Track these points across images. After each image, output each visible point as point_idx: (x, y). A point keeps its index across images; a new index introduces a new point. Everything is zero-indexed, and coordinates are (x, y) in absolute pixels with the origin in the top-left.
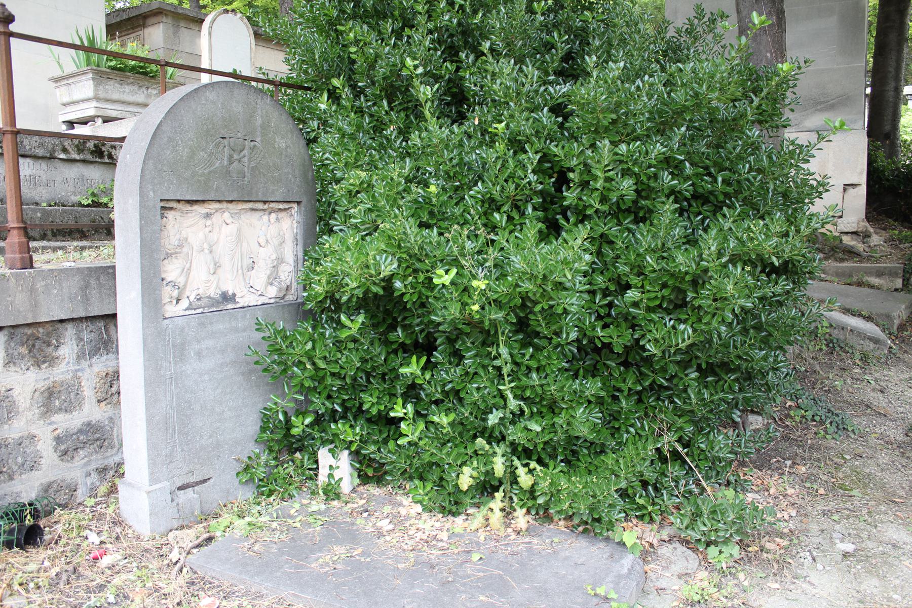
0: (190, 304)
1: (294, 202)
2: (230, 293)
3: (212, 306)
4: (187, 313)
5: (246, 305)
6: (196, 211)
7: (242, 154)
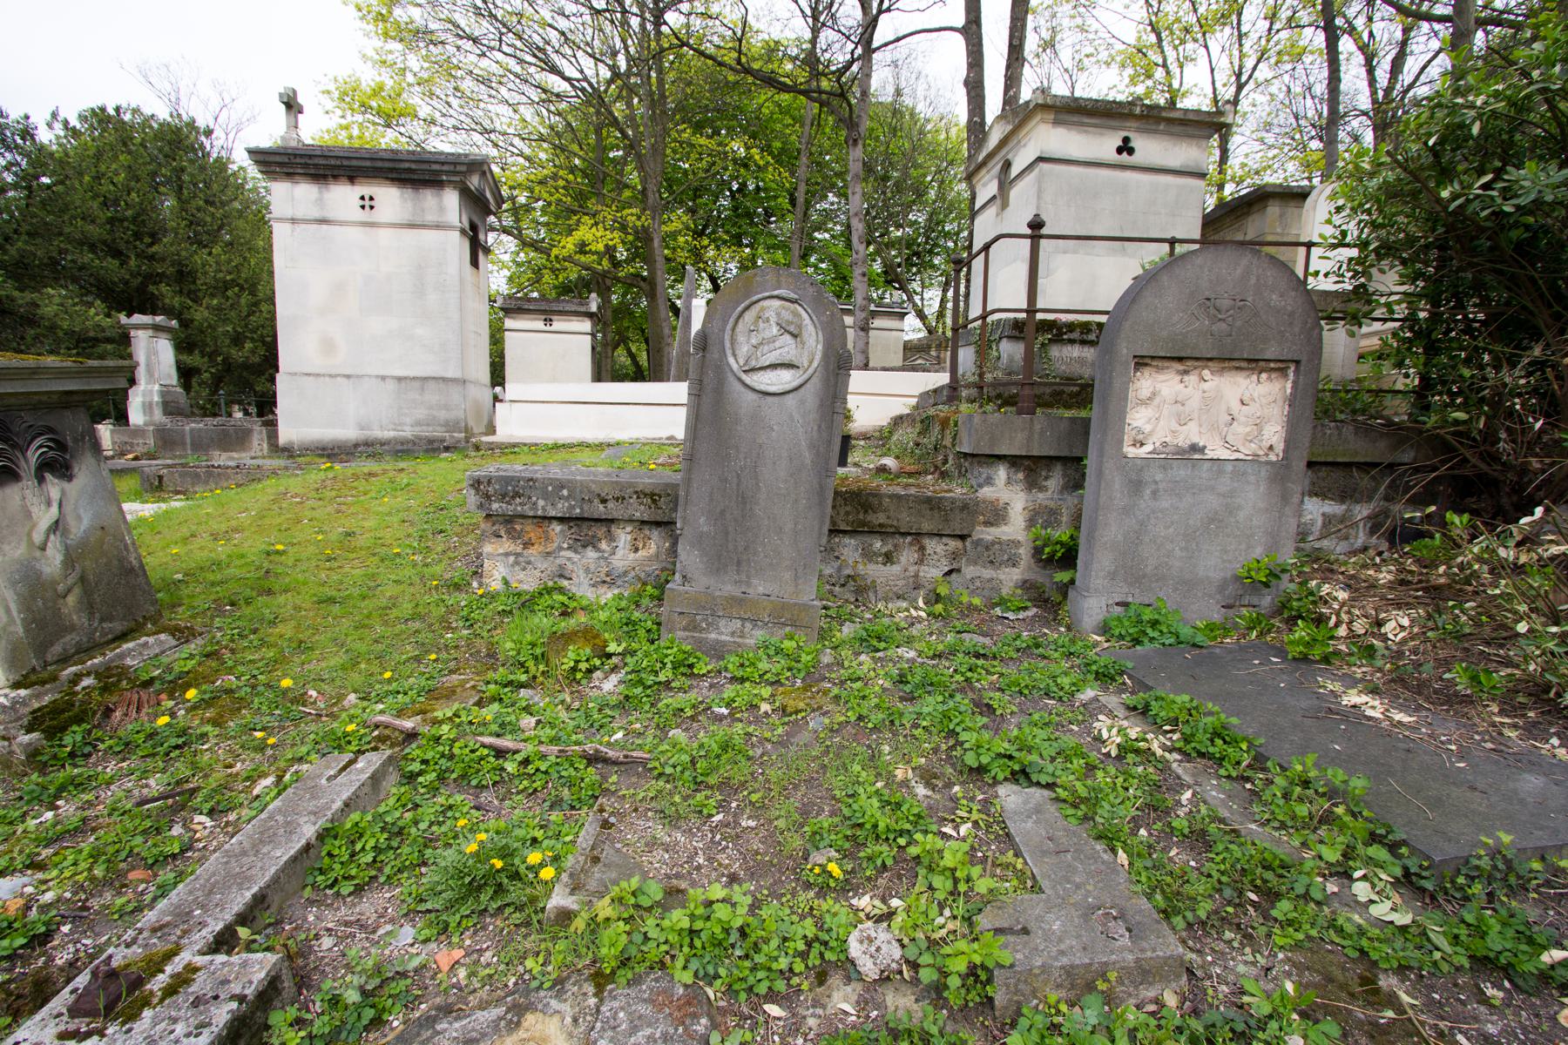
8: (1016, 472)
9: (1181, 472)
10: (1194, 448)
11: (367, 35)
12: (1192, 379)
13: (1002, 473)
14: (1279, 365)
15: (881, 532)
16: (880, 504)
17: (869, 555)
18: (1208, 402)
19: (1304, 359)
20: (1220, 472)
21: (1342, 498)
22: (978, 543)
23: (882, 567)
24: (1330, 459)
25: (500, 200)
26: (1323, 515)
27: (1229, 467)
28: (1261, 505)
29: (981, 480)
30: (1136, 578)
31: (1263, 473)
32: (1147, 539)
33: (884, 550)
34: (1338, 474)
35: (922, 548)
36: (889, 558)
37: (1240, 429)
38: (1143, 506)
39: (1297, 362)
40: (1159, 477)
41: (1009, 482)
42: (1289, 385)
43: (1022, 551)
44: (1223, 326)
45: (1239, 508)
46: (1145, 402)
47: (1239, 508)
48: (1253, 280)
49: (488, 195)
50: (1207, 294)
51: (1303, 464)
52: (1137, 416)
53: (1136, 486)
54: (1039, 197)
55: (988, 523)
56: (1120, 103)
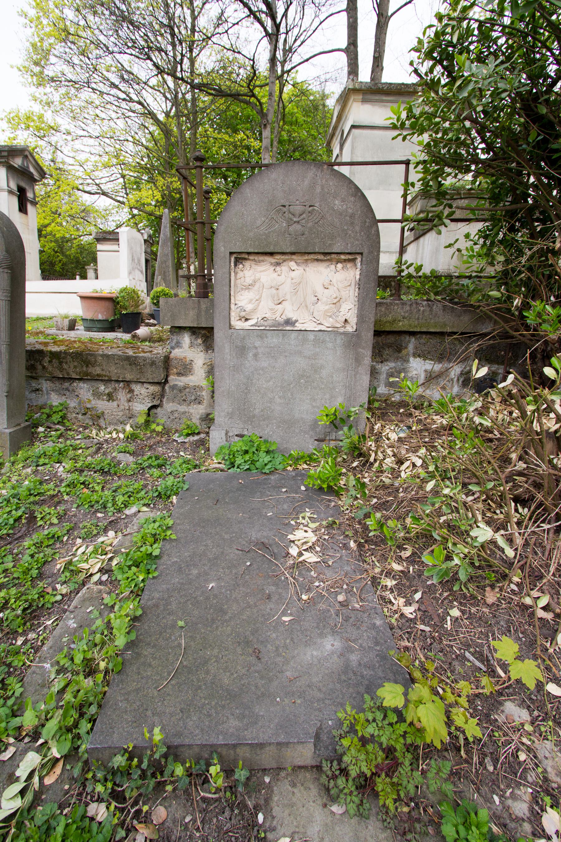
0: (257, 323)
1: (358, 253)
2: (294, 319)
3: (274, 326)
4: (252, 328)
5: (303, 329)
6: (266, 261)
7: (302, 217)
8: (196, 339)
9: (274, 340)
10: (288, 322)
11: (24, 85)
12: (284, 268)
13: (186, 339)
14: (350, 257)
15: (98, 379)
16: (96, 361)
17: (97, 395)
18: (297, 286)
19: (366, 251)
20: (305, 341)
21: (440, 358)
22: (174, 387)
23: (107, 403)
24: (424, 330)
25: (43, 174)
26: (426, 371)
27: (311, 336)
28: (339, 365)
29: (173, 344)
30: (250, 419)
31: (339, 341)
32: (253, 390)
33: (107, 391)
34: (434, 341)
35: (131, 391)
36: (110, 397)
37: (322, 307)
38: (248, 365)
39: (361, 254)
40: (258, 344)
41: (191, 345)
42: (358, 272)
43: (204, 393)
44: (298, 227)
45: (322, 367)
46: (248, 287)
47: (322, 367)
48: (318, 189)
49: (32, 170)
50: (283, 202)
51: (371, 334)
52: (242, 298)
53: (242, 351)
54: (352, 153)
55: (179, 374)
56: (407, 85)
